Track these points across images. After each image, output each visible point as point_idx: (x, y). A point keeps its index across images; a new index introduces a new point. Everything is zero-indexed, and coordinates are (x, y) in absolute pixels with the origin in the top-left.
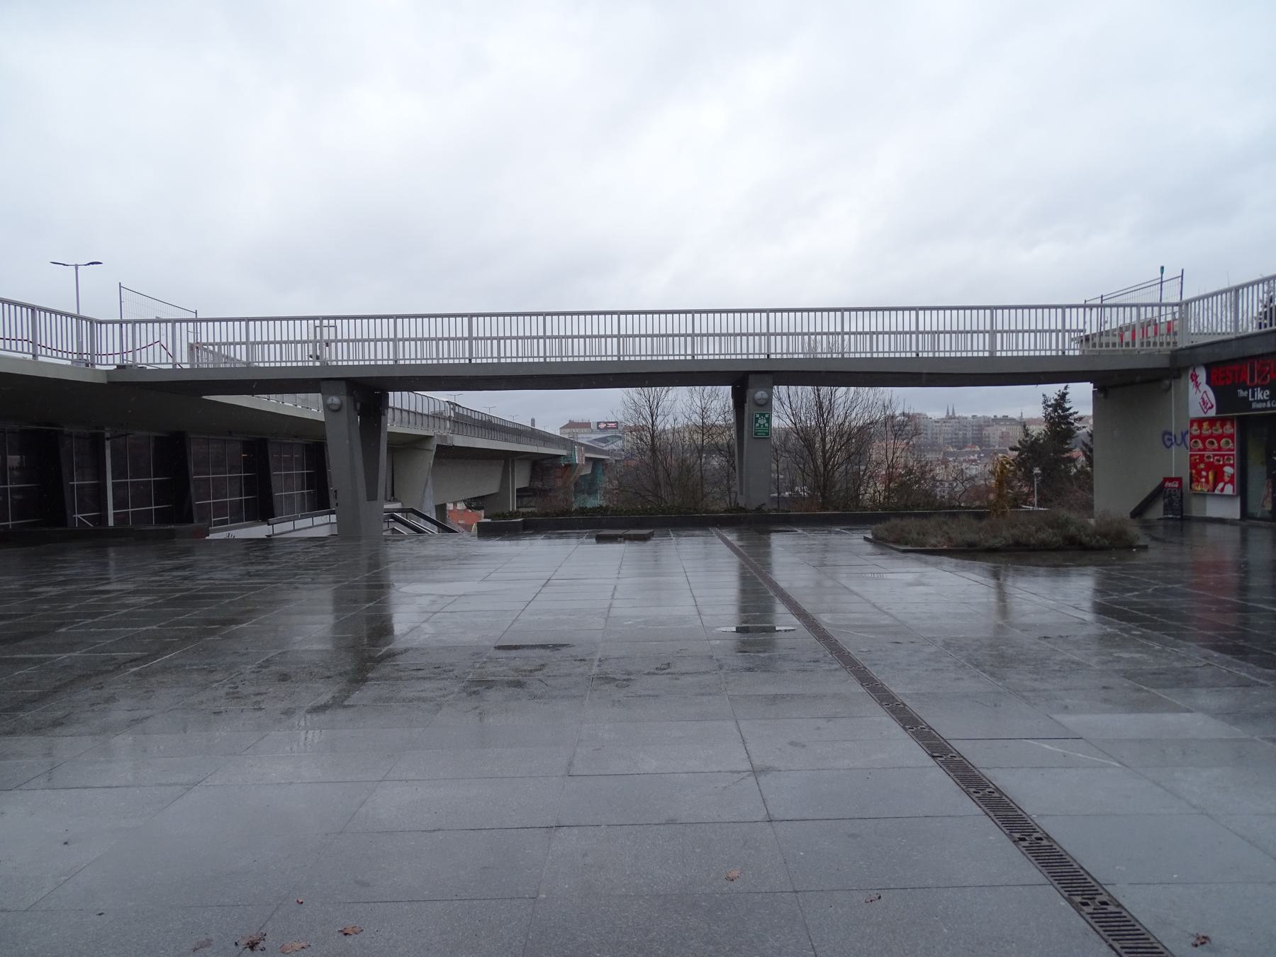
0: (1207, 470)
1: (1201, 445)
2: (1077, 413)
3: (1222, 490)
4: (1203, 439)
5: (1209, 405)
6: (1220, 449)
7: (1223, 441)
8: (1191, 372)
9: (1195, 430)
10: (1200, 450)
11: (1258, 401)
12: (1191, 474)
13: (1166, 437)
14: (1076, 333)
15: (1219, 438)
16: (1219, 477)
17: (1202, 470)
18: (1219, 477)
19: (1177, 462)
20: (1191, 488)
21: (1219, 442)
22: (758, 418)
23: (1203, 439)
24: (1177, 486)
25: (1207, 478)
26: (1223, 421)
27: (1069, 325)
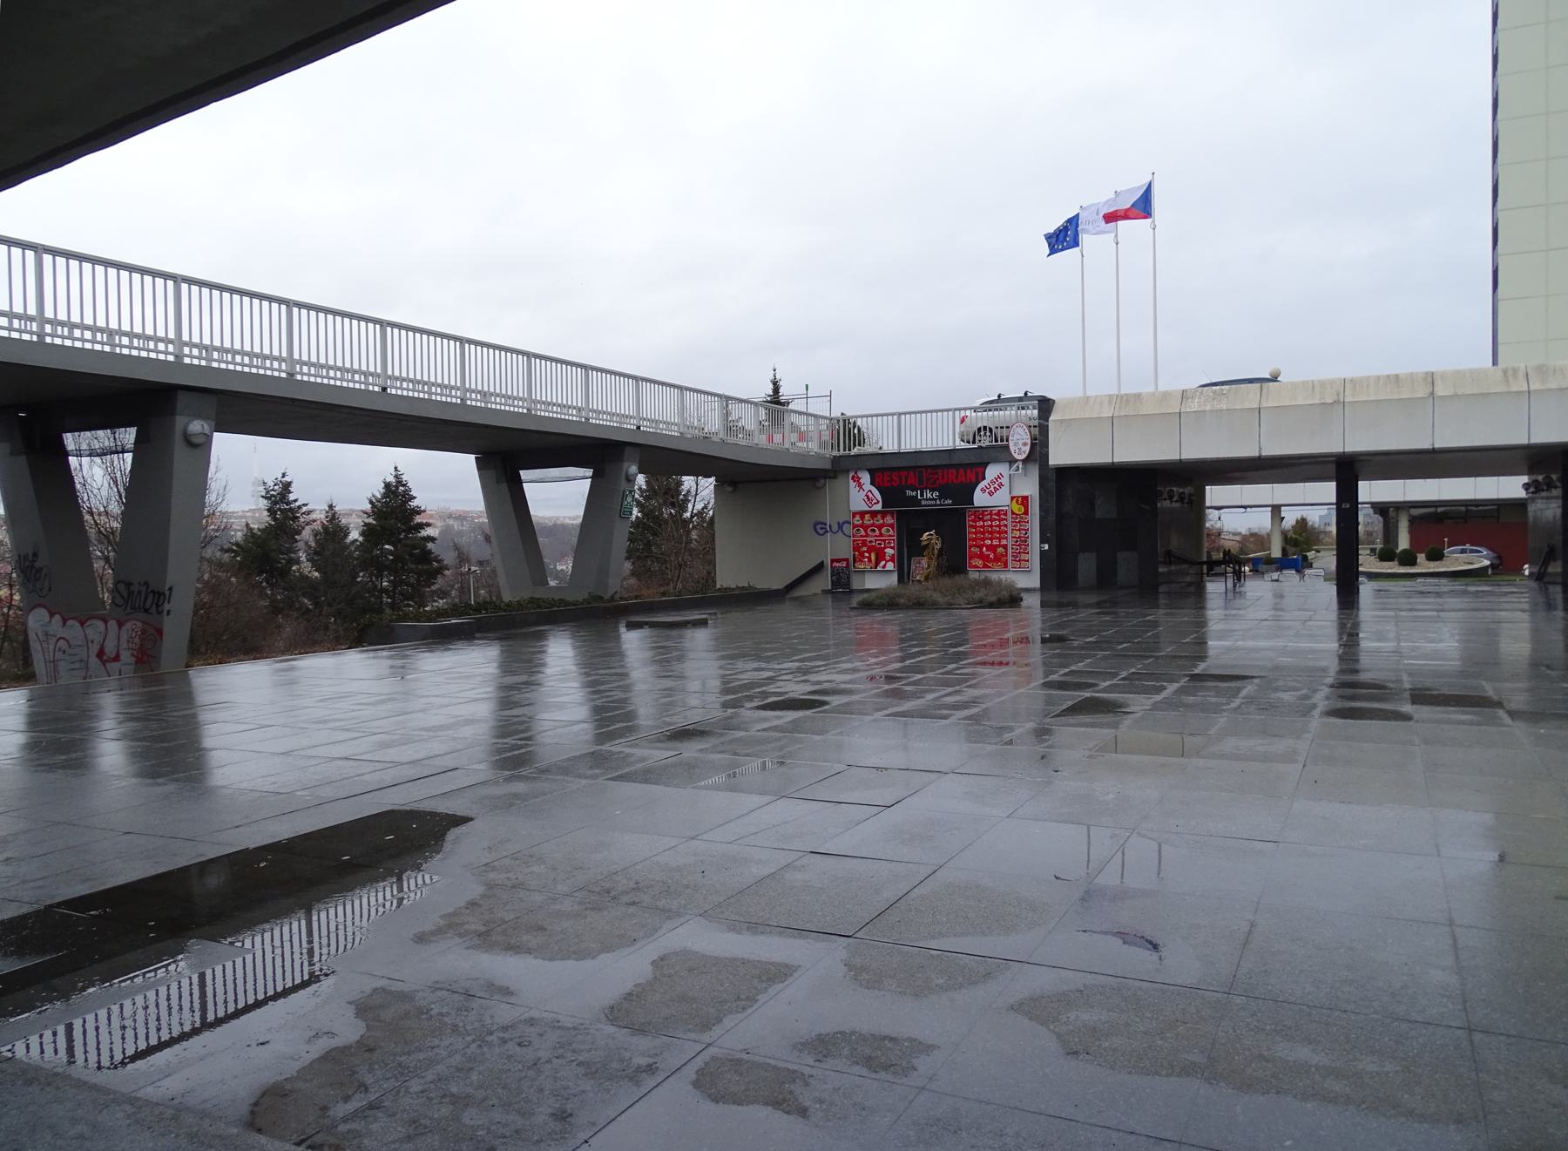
0: (869, 551)
1: (863, 533)
2: (307, 505)
3: (884, 567)
4: (866, 528)
5: (875, 501)
6: (881, 535)
7: (884, 530)
8: (852, 474)
9: (857, 520)
10: (862, 536)
11: (927, 500)
12: (854, 555)
13: (818, 527)
14: (350, 374)
15: (880, 527)
16: (881, 556)
17: (865, 552)
18: (881, 556)
19: (837, 547)
20: (854, 566)
21: (880, 531)
22: (627, 496)
23: (866, 528)
24: (844, 565)
25: (869, 558)
26: (883, 514)
27: (269, 349)
